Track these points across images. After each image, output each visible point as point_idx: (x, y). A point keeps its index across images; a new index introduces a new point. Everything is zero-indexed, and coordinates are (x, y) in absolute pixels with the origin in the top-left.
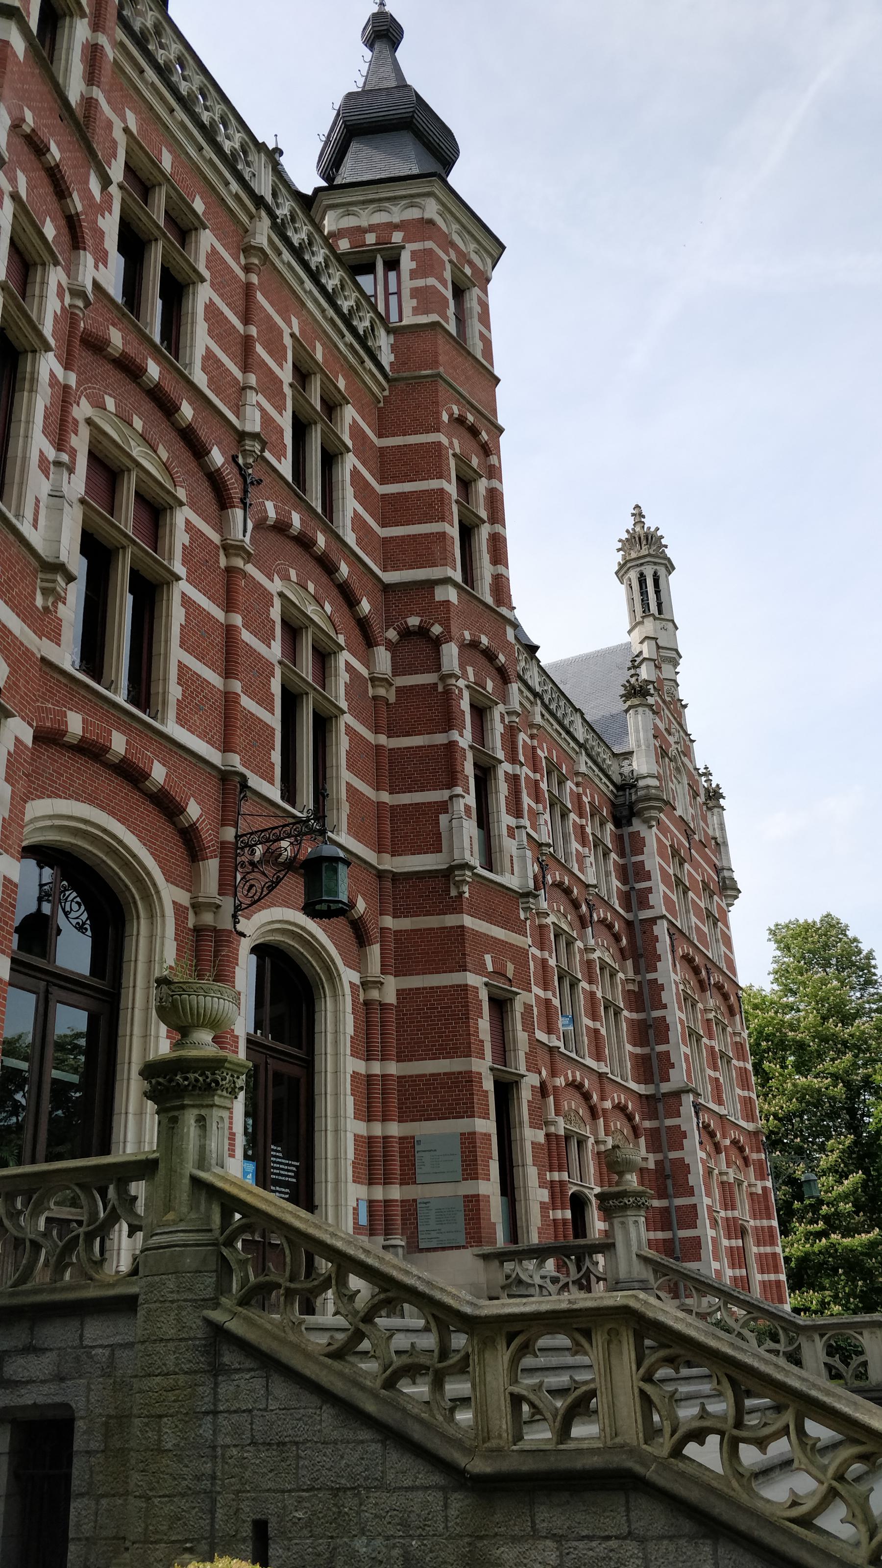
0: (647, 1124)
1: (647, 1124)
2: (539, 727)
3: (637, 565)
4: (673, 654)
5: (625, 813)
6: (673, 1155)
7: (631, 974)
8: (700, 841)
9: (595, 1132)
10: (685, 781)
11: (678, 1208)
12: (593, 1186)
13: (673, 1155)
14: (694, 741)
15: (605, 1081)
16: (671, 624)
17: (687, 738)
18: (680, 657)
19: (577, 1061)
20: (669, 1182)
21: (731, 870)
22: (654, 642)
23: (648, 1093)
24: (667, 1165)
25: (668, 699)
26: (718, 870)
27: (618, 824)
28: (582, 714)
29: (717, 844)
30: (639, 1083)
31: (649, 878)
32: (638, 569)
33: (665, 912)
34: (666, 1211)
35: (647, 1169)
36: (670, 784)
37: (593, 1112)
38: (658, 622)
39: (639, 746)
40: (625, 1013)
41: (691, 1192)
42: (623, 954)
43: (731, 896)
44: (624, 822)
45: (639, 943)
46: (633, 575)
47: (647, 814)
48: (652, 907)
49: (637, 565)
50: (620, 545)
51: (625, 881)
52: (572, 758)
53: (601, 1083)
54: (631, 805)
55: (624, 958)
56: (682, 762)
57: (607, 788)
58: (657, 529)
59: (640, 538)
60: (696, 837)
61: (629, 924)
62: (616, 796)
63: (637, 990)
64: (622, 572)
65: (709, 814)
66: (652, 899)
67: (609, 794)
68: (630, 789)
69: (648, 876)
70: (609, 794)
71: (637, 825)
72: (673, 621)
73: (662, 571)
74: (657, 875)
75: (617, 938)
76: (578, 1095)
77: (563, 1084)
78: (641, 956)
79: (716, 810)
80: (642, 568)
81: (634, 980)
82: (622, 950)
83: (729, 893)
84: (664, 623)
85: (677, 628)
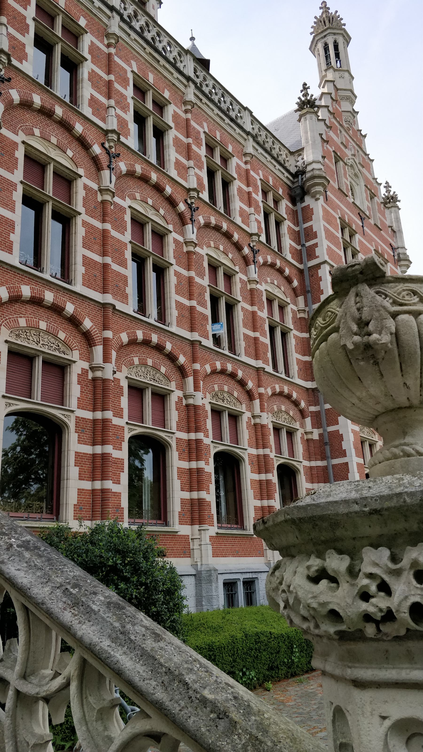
0: (312, 409)
1: (312, 409)
2: (193, 105)
3: (322, 38)
4: (349, 94)
5: (298, 191)
6: (331, 429)
7: (302, 305)
8: (375, 224)
9: (303, 425)
10: (363, 184)
11: (334, 466)
12: (301, 460)
13: (331, 429)
14: (373, 160)
15: (198, 347)
16: (346, 74)
17: (366, 157)
18: (356, 97)
19: (286, 380)
20: (328, 448)
21: (404, 248)
22: (332, 84)
23: (313, 387)
24: (326, 435)
25: (346, 126)
26: (393, 249)
27: (293, 201)
28: (251, 113)
29: (394, 232)
30: (307, 381)
31: (316, 237)
32: (323, 40)
33: (327, 258)
34: (325, 468)
35: (312, 439)
36: (344, 180)
37: (250, 395)
38: (337, 73)
39: (307, 142)
40: (295, 332)
41: (343, 454)
42: (295, 293)
43: (404, 265)
44: (298, 199)
45: (307, 282)
46: (320, 46)
47: (313, 190)
48: (318, 257)
49: (322, 38)
50: (312, 30)
51: (299, 242)
52: (241, 144)
53: (258, 375)
54: (302, 187)
55: (297, 296)
56: (359, 170)
57: (285, 176)
58: (336, 12)
59: (324, 22)
60: (372, 221)
61: (301, 272)
62: (293, 183)
63: (307, 317)
64: (313, 48)
65: (387, 211)
66: (318, 251)
67: (285, 180)
68: (302, 175)
69: (315, 236)
70: (285, 180)
71: (308, 201)
72: (348, 71)
73: (341, 41)
74: (322, 234)
75: (289, 280)
76: (282, 399)
77: (270, 393)
78: (308, 292)
79: (393, 209)
80: (325, 39)
81: (304, 311)
82: (294, 290)
83: (402, 263)
84: (342, 73)
85: (353, 78)
